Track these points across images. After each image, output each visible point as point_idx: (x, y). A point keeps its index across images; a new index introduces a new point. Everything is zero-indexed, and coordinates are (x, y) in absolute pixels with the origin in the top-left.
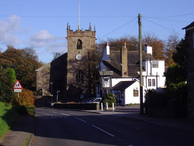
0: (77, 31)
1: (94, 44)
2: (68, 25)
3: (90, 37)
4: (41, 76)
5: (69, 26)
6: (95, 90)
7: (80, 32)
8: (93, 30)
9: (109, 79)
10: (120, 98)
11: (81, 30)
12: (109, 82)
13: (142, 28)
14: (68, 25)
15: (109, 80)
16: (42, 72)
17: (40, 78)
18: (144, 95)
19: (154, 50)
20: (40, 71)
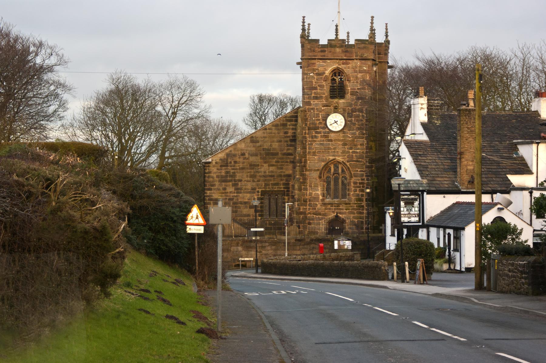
0: (331, 44)
1: (50, 69)
2: (304, 22)
3: (370, 63)
4: (217, 177)
5: (306, 27)
6: (520, 97)
7: (341, 46)
8: (380, 39)
9: (416, 200)
10: (452, 249)
11: (343, 41)
12: (417, 209)
13: (416, 339)
14: (304, 22)
15: (416, 203)
16: (221, 166)
17: (217, 183)
18: (533, 202)
19: (373, 69)
20: (216, 163)
